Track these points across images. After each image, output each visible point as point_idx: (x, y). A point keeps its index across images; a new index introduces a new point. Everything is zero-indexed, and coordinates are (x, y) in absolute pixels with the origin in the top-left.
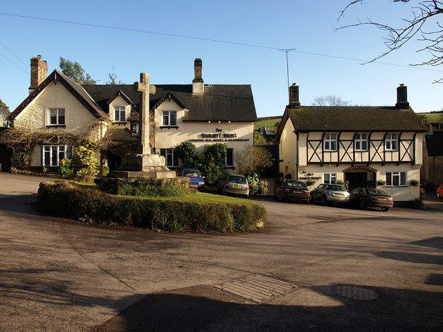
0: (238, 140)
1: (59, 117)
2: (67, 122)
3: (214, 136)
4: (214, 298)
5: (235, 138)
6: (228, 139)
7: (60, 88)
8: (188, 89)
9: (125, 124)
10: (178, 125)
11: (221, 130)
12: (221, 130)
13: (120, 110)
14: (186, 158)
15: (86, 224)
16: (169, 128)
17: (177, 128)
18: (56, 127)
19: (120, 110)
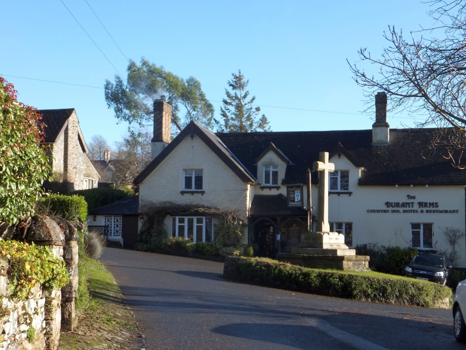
0: (441, 212)
1: (196, 177)
2: (205, 187)
3: (404, 205)
4: (230, 337)
5: (435, 209)
6: (425, 209)
7: (198, 143)
8: (365, 135)
9: (278, 188)
10: (350, 190)
11: (414, 198)
12: (414, 198)
13: (271, 170)
14: (457, 70)
15: (149, 252)
16: (339, 194)
17: (350, 194)
18: (192, 193)
19: (271, 170)
